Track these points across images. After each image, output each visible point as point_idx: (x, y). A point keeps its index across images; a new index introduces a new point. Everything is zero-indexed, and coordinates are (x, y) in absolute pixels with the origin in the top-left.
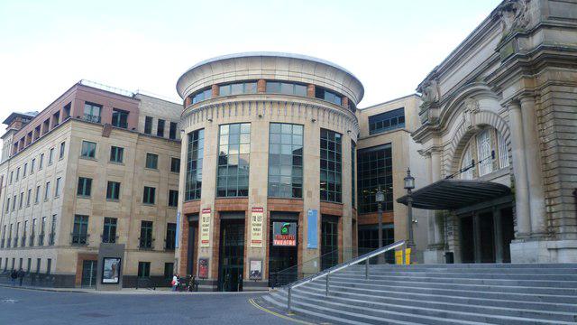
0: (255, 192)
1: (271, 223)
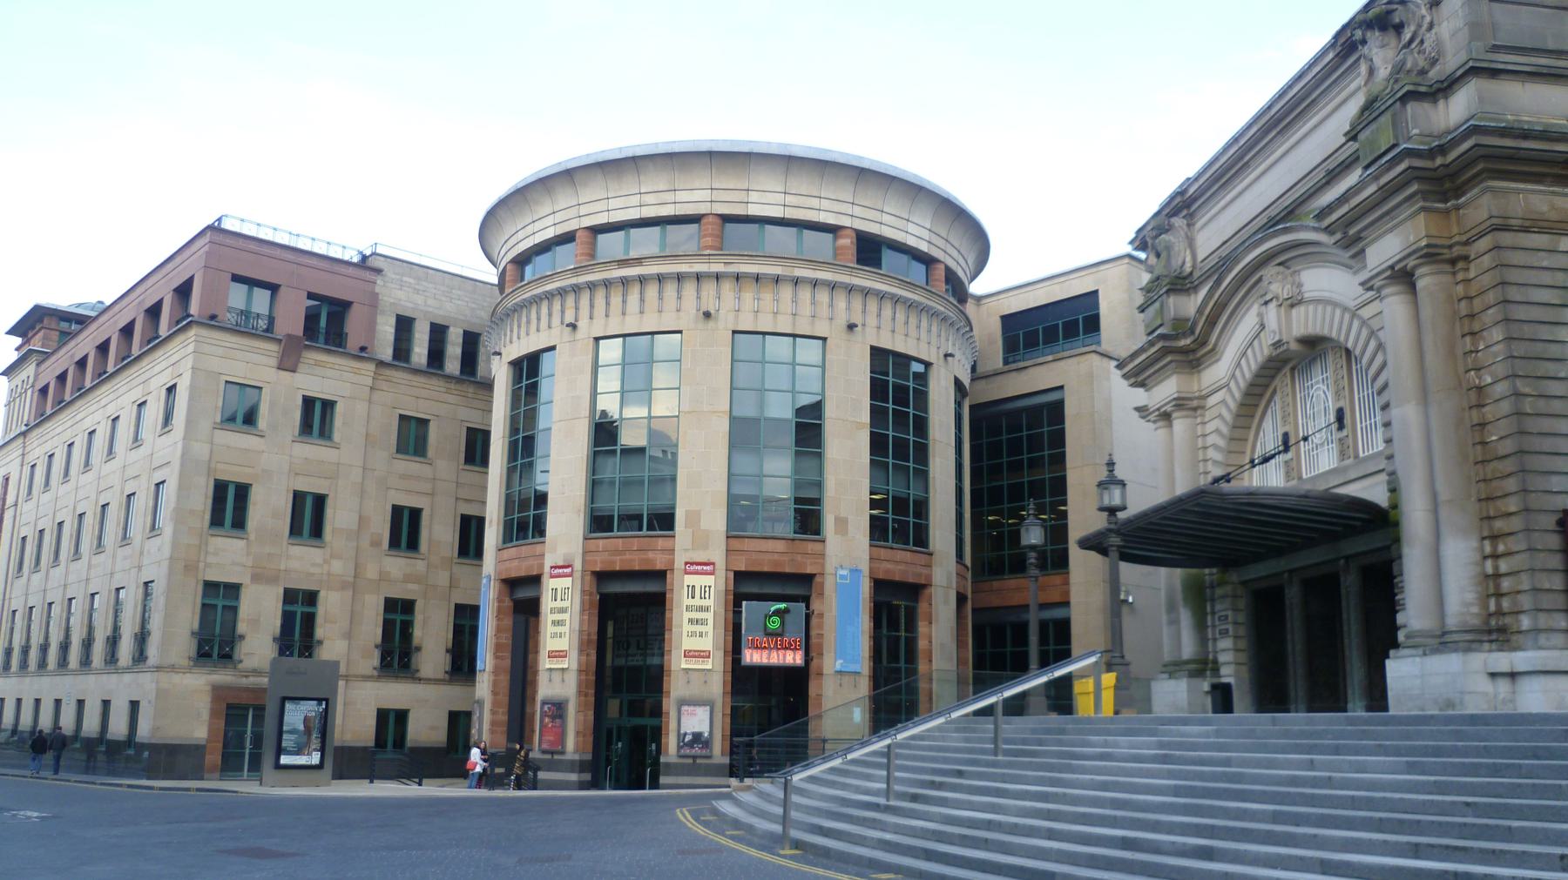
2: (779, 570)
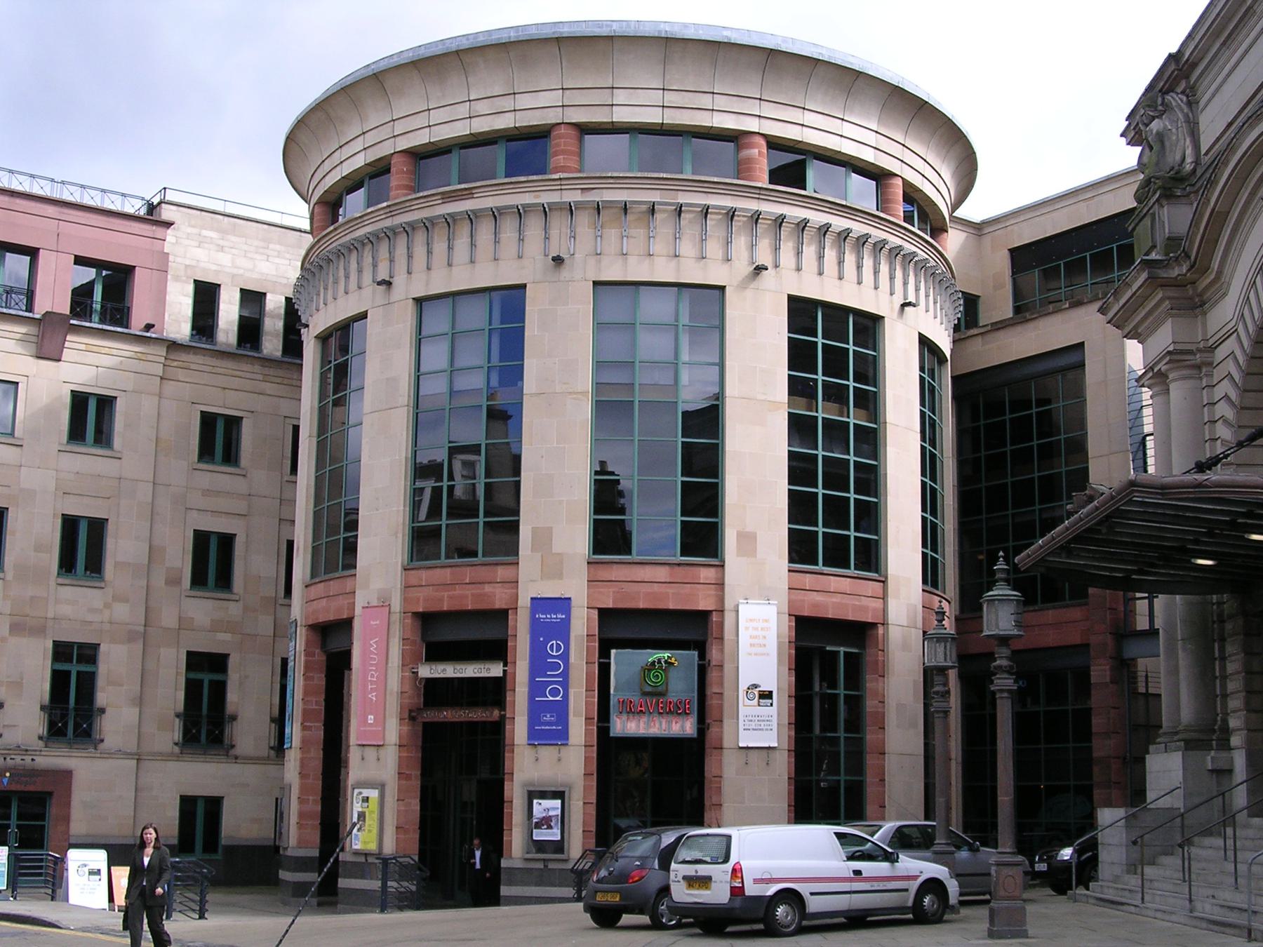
0: (543, 537)
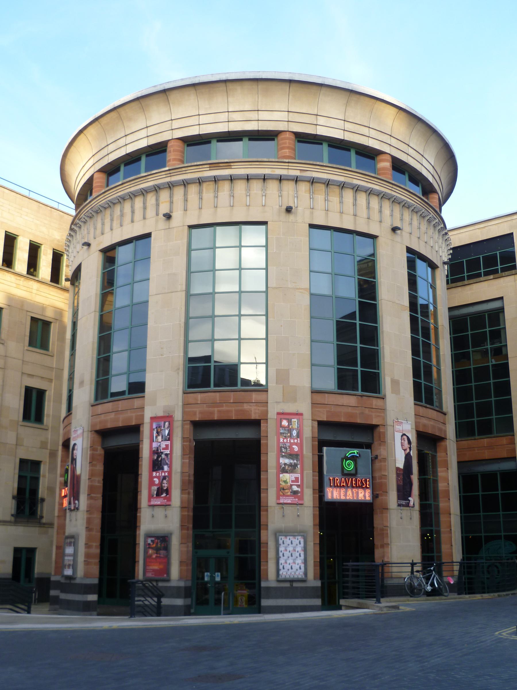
1: (320, 450)
2: (352, 420)
